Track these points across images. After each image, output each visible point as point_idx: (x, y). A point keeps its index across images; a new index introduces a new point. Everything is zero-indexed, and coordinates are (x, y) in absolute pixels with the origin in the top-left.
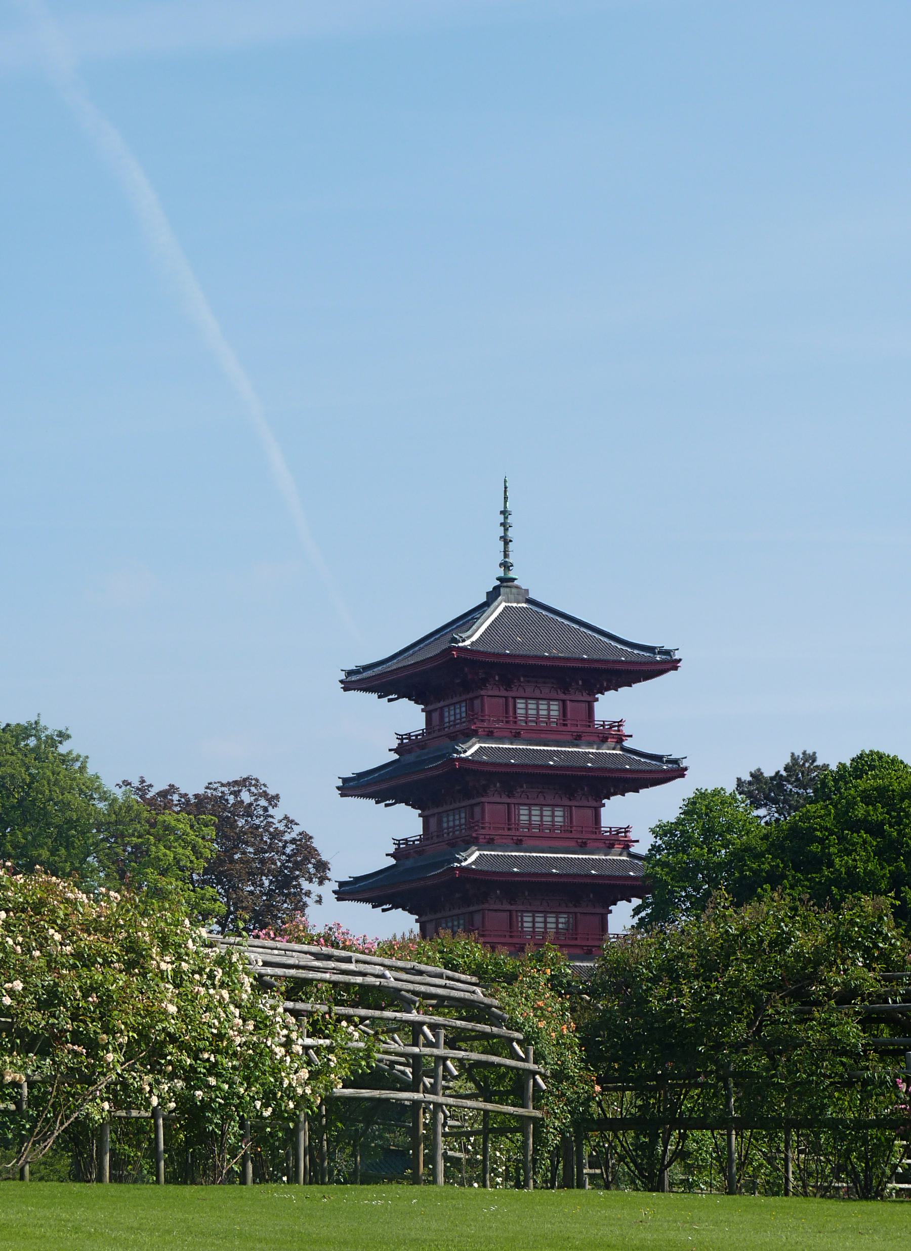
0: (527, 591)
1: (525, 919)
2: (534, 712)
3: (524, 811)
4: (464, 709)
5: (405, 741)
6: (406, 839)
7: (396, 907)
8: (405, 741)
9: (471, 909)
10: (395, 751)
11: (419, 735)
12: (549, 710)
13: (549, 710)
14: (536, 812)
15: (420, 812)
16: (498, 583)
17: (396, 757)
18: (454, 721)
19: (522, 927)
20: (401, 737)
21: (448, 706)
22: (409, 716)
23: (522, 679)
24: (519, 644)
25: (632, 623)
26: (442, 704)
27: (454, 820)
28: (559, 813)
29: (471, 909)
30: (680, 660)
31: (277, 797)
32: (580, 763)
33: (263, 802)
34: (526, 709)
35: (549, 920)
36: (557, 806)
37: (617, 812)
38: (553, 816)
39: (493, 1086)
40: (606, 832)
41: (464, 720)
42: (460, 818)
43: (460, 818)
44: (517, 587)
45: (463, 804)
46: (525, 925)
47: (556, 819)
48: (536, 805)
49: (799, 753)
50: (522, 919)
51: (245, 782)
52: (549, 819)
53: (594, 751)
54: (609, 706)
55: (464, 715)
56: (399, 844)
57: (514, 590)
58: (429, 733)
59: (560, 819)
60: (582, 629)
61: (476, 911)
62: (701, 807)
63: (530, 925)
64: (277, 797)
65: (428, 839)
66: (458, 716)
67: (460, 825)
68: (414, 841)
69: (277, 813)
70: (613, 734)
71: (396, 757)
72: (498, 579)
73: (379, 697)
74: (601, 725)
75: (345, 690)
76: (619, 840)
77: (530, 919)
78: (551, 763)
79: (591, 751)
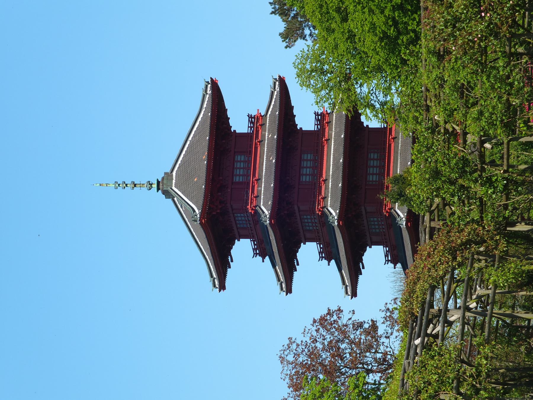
0: (165, 173)
1: (371, 179)
2: (242, 164)
3: (304, 179)
4: (239, 215)
5: (258, 252)
6: (319, 253)
7: (361, 261)
8: (258, 252)
9: (364, 213)
10: (264, 258)
11: (254, 243)
12: (240, 161)
13: (240, 161)
14: (305, 164)
15: (302, 244)
16: (160, 191)
17: (267, 258)
18: (246, 221)
19: (376, 181)
20: (255, 254)
21: (236, 224)
22: (242, 249)
23: (221, 178)
24: (200, 180)
25: (188, 113)
26: (235, 228)
27: (308, 222)
28: (305, 157)
29: (364, 213)
30: (211, 78)
31: (290, 339)
32: (275, 142)
33: (294, 346)
34: (240, 175)
35: (372, 164)
36: (301, 157)
37: (305, 121)
38: (307, 160)
39: (491, 15)
40: (318, 127)
41: (245, 215)
42: (307, 219)
43: (307, 219)
44: (163, 178)
45: (298, 218)
46: (374, 179)
47: (309, 158)
48: (300, 179)
49: (270, 9)
50: (371, 181)
51: (282, 359)
52: (309, 162)
53: (267, 134)
54: (239, 124)
55: (242, 215)
56: (322, 257)
57: (165, 182)
58: (253, 237)
59: (309, 155)
60: (190, 139)
61: (366, 210)
62: (305, 76)
63: (375, 169)
64: (290, 339)
65: (320, 240)
66: (243, 218)
67: (311, 219)
68: (321, 248)
69: (299, 338)
70: (256, 121)
71: (267, 258)
72: (158, 191)
73: (230, 267)
74: (251, 129)
75: (225, 289)
76: (322, 119)
77: (371, 169)
78: (274, 161)
79: (267, 135)
